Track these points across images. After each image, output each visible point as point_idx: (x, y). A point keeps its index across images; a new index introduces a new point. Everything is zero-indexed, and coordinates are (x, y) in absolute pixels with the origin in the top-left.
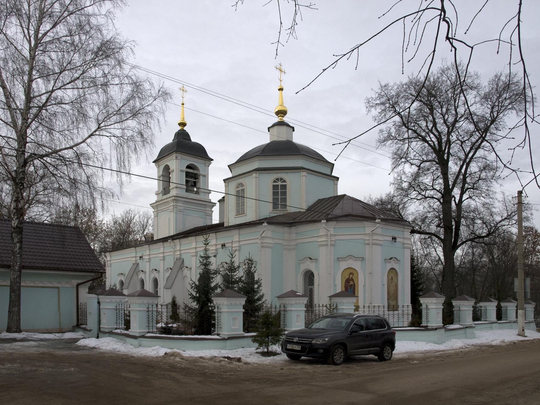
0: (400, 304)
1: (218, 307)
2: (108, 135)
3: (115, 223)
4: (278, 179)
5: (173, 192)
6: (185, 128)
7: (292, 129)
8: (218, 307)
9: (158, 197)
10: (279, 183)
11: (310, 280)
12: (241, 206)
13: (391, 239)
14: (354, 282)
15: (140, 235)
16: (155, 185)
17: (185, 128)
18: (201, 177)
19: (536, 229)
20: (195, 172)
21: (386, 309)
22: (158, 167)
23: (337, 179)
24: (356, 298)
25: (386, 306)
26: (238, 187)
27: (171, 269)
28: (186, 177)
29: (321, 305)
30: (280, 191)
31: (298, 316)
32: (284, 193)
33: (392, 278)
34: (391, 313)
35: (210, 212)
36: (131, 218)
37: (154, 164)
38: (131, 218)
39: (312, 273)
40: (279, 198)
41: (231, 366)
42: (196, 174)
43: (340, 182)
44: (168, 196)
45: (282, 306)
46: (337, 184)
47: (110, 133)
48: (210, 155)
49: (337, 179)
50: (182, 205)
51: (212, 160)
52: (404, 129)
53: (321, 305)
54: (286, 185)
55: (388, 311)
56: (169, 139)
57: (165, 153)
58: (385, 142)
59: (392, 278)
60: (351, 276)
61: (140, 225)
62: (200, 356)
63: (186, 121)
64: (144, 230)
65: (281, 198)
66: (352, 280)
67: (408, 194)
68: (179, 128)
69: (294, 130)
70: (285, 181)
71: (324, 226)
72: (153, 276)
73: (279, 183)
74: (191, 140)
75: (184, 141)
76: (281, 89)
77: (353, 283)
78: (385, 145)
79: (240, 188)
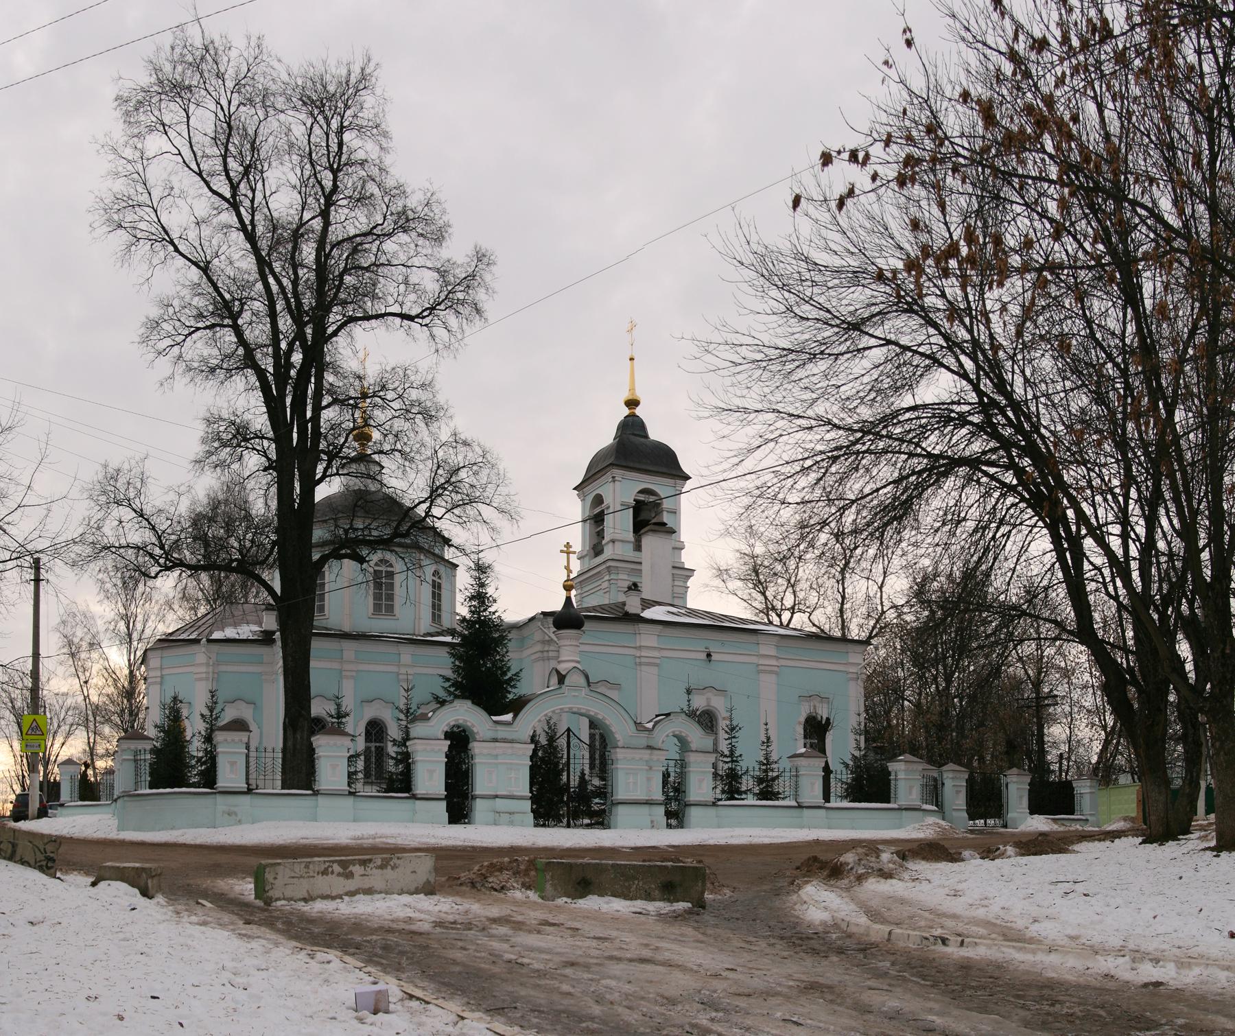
5: (608, 552)
6: (638, 411)
9: (582, 565)
10: (383, 568)
16: (576, 537)
17: (638, 411)
18: (665, 513)
22: (583, 497)
24: (247, 734)
29: (270, 749)
31: (431, 772)
35: (681, 590)
37: (576, 492)
45: (794, 770)
48: (685, 467)
50: (625, 577)
51: (687, 478)
53: (270, 749)
56: (606, 437)
57: (598, 469)
62: (993, 911)
63: (639, 395)
65: (375, 741)
68: (626, 411)
70: (391, 566)
71: (203, 649)
73: (383, 568)
74: (646, 437)
75: (633, 438)
76: (632, 359)
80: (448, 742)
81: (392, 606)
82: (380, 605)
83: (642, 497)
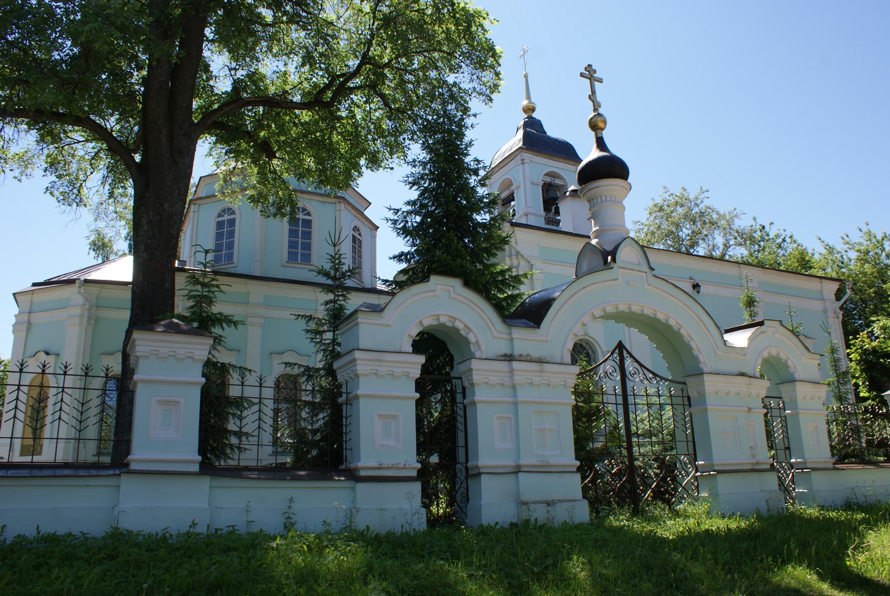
26: (220, 215)
46: (375, 237)
54: (311, 220)
65: (298, 249)
70: (309, 214)
79: (226, 217)
80: (421, 359)
81: (310, 244)
82: (297, 243)
83: (548, 179)
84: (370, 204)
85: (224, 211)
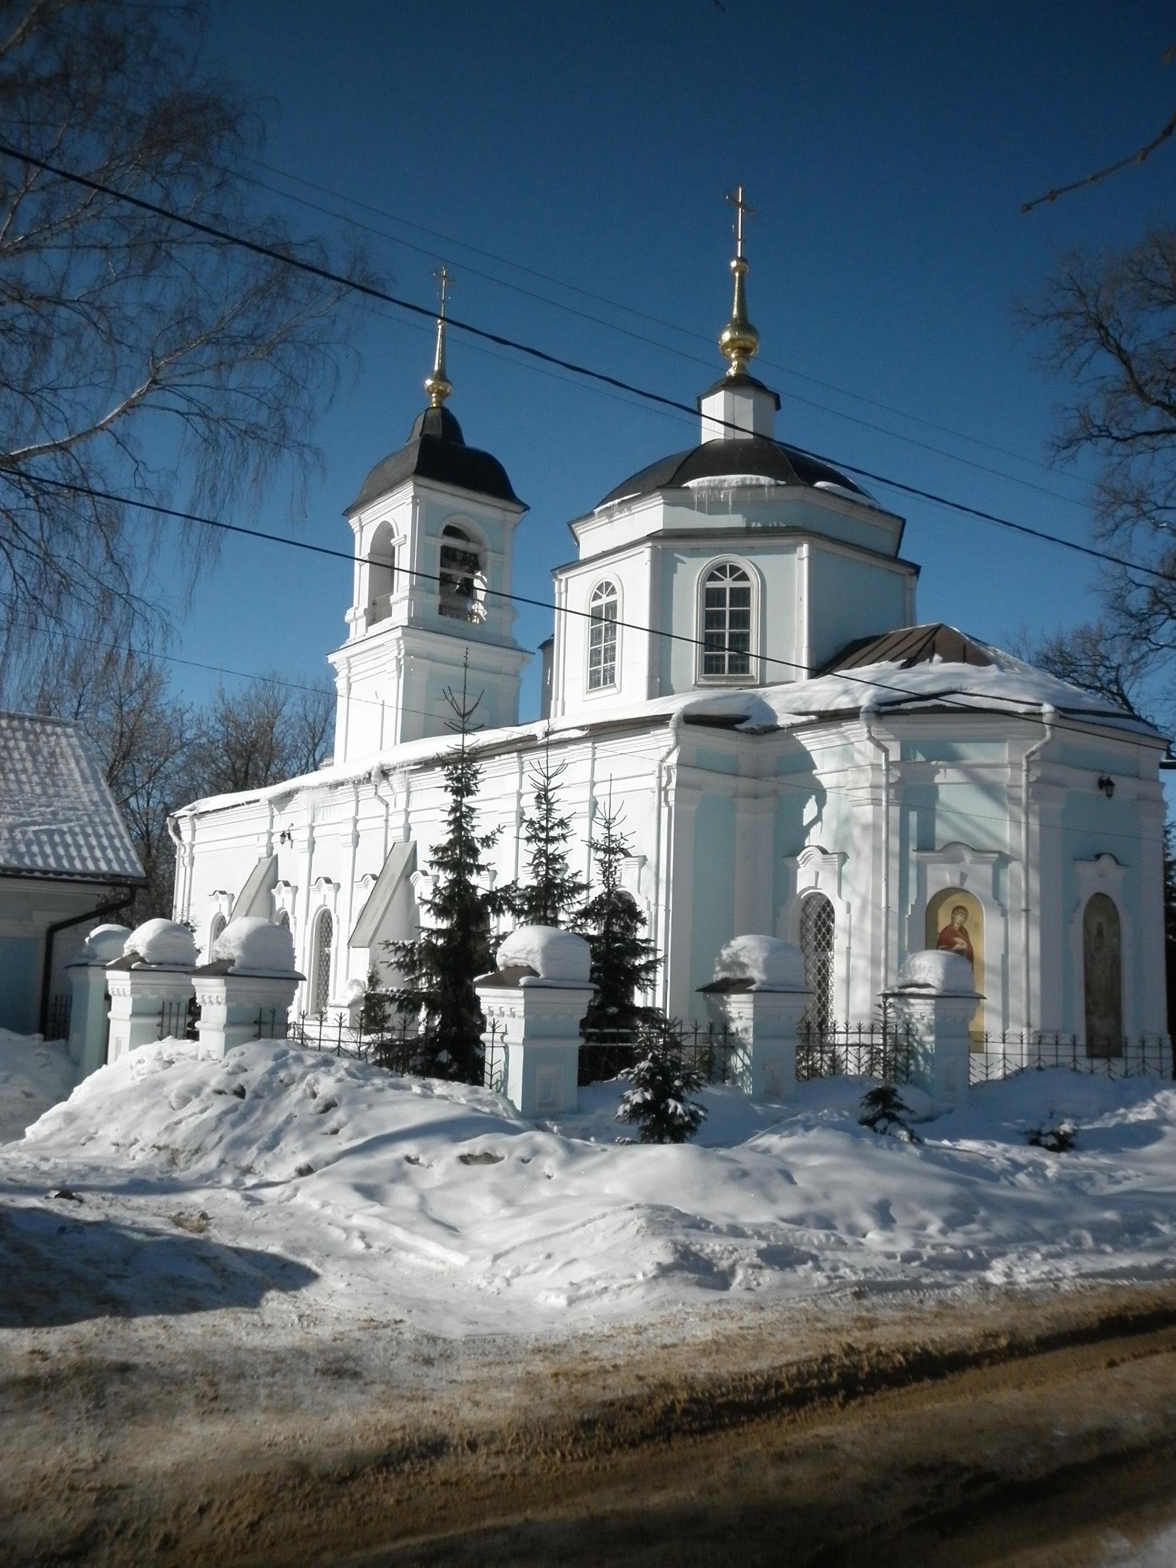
0: (1130, 1030)
1: (494, 1026)
2: (182, 405)
3: (224, 719)
4: (721, 569)
7: (771, 403)
8: (494, 1026)
10: (727, 583)
11: (819, 930)
12: (605, 662)
13: (1091, 778)
14: (968, 942)
15: (301, 760)
19: (699, 1128)
20: (472, 548)
21: (1081, 1051)
23: (916, 570)
25: (1082, 1040)
26: (596, 597)
27: (374, 877)
28: (442, 565)
30: (727, 609)
32: (741, 619)
33: (1100, 932)
34: (1097, 1063)
36: (275, 705)
38: (275, 705)
39: (828, 903)
40: (724, 634)
41: (805, 1115)
42: (476, 556)
43: (923, 584)
44: (385, 624)
46: (912, 590)
47: (190, 400)
49: (916, 570)
52: (1134, 401)
55: (1091, 1055)
58: (1074, 448)
59: (1100, 932)
60: (959, 918)
61: (302, 728)
64: (316, 745)
65: (731, 635)
66: (963, 933)
67: (1148, 631)
69: (778, 406)
70: (744, 577)
72: (316, 902)
74: (462, 441)
77: (965, 946)
78: (1073, 458)
79: (605, 600)
84: (904, 521)
85: (600, 588)
